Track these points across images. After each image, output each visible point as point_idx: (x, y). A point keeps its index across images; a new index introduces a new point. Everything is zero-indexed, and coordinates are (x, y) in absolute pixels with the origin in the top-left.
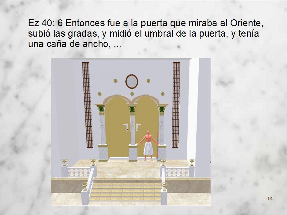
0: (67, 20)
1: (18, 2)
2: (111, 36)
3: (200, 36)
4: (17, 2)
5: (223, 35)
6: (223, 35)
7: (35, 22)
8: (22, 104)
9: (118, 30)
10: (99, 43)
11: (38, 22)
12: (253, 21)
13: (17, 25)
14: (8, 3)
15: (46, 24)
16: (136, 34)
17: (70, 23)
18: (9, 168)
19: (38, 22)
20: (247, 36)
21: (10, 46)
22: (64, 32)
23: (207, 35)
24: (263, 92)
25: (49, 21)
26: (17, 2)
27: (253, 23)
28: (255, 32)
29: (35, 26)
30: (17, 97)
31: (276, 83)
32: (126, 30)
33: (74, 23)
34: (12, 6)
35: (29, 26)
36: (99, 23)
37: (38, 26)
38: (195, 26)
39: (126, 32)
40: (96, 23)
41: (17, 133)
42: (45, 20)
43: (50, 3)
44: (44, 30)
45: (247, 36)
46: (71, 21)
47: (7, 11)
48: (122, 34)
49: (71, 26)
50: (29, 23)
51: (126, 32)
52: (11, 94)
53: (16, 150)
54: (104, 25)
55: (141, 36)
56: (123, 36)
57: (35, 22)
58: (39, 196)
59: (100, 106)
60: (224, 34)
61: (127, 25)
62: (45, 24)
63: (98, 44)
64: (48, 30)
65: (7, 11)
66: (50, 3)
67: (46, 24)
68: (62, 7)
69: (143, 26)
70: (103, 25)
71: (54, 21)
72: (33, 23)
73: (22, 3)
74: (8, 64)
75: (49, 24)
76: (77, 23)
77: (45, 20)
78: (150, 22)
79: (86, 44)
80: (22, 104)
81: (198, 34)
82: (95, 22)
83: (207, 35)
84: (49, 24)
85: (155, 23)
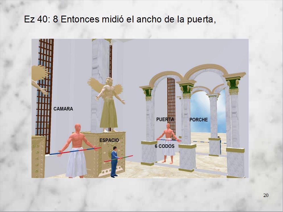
0: (25, 16)
1: (18, 2)
2: (103, 22)
3: (188, 21)
4: (17, 2)
5: (210, 21)
6: (210, 21)
7: (31, 18)
8: (22, 102)
9: (111, 16)
10: (153, 18)
11: (34, 18)
12: (72, 17)
13: (17, 25)
14: (9, 3)
15: (42, 20)
16: (127, 20)
17: (65, 19)
18: (9, 166)
19: (34, 18)
20: (204, 22)
21: (11, 46)
22: (98, 18)
23: (195, 20)
24: (260, 91)
25: (45, 17)
26: (17, 2)
27: (72, 19)
28: (181, 18)
29: (31, 22)
30: (17, 95)
31: (272, 81)
32: (118, 16)
33: (69, 19)
34: (13, 6)
35: (25, 22)
36: (94, 20)
37: (34, 22)
38: (71, 22)
39: (118, 18)
40: (90, 20)
41: (17, 131)
42: (41, 17)
43: (50, 3)
44: (111, 16)
45: (204, 22)
46: (66, 18)
47: (7, 10)
48: (114, 20)
49: (66, 22)
50: (25, 19)
51: (118, 18)
52: (11, 93)
53: (16, 147)
54: (98, 22)
55: (133, 22)
56: (116, 21)
57: (31, 18)
58: (38, 192)
59: (143, 87)
60: (212, 19)
61: (212, 22)
62: (41, 20)
63: (151, 20)
64: (122, 16)
65: (7, 10)
66: (50, 3)
67: (42, 20)
68: (61, 7)
69: (167, 18)
70: (98, 21)
71: (49, 18)
72: (29, 19)
73: (22, 3)
74: (8, 63)
75: (45, 21)
76: (72, 19)
77: (41, 17)
78: (196, 18)
79: (140, 19)
80: (22, 102)
81: (186, 20)
82: (90, 19)
83: (195, 20)
84: (45, 21)
85: (201, 20)
